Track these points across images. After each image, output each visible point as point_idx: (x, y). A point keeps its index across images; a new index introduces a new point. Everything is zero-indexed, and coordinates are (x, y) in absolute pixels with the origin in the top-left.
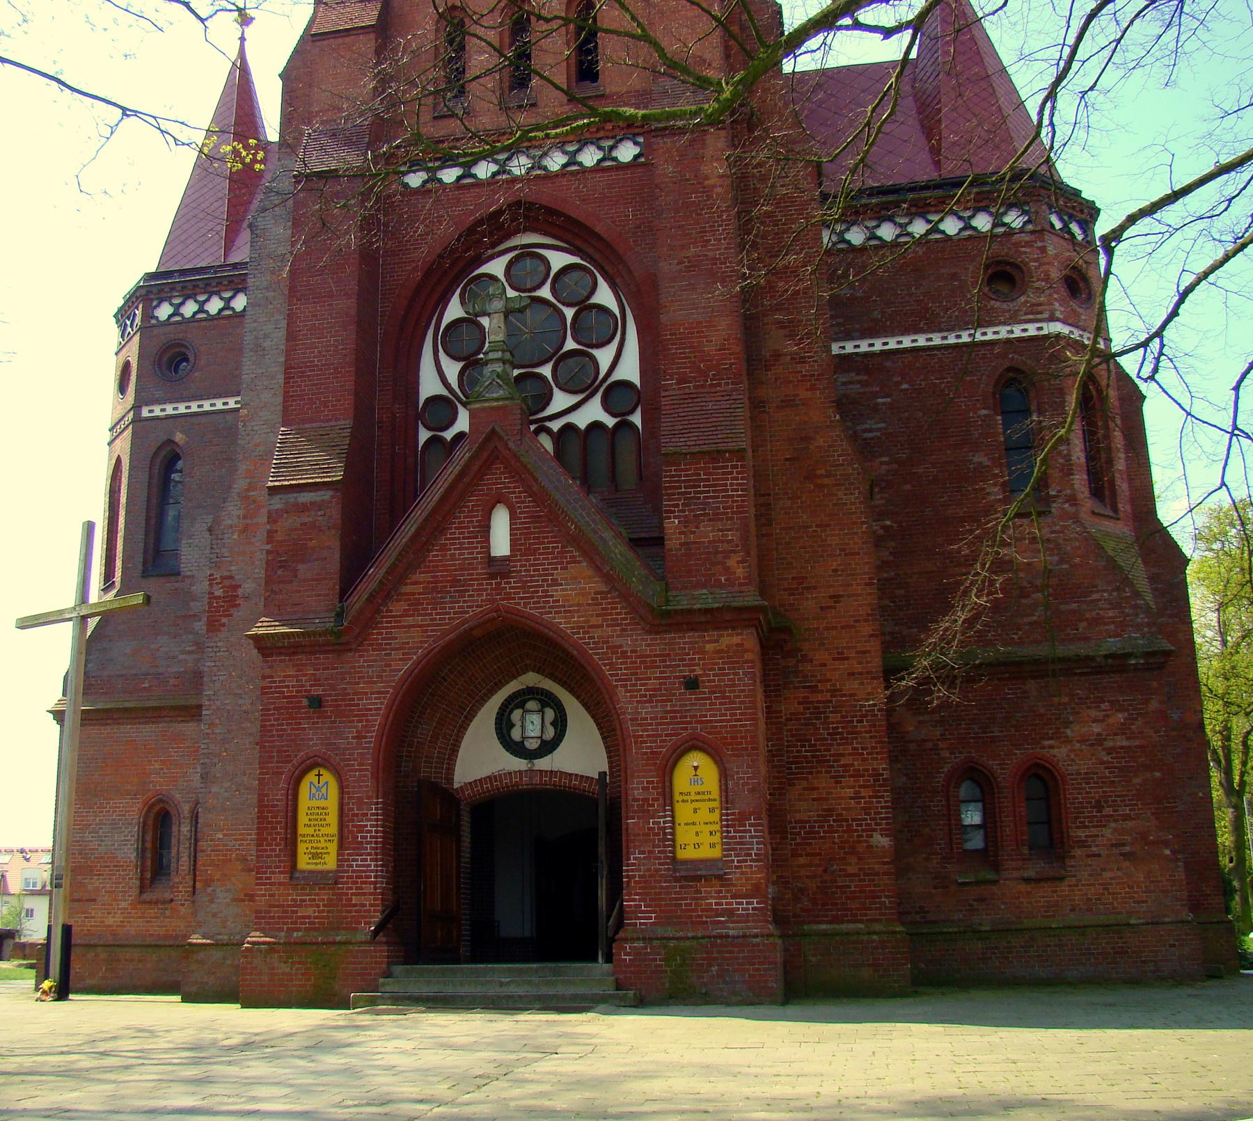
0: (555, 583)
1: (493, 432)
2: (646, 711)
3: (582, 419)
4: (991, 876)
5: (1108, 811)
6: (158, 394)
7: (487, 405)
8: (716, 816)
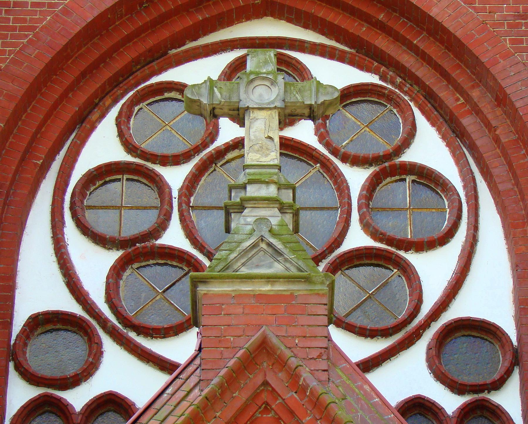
1: (264, 347)
7: (246, 288)
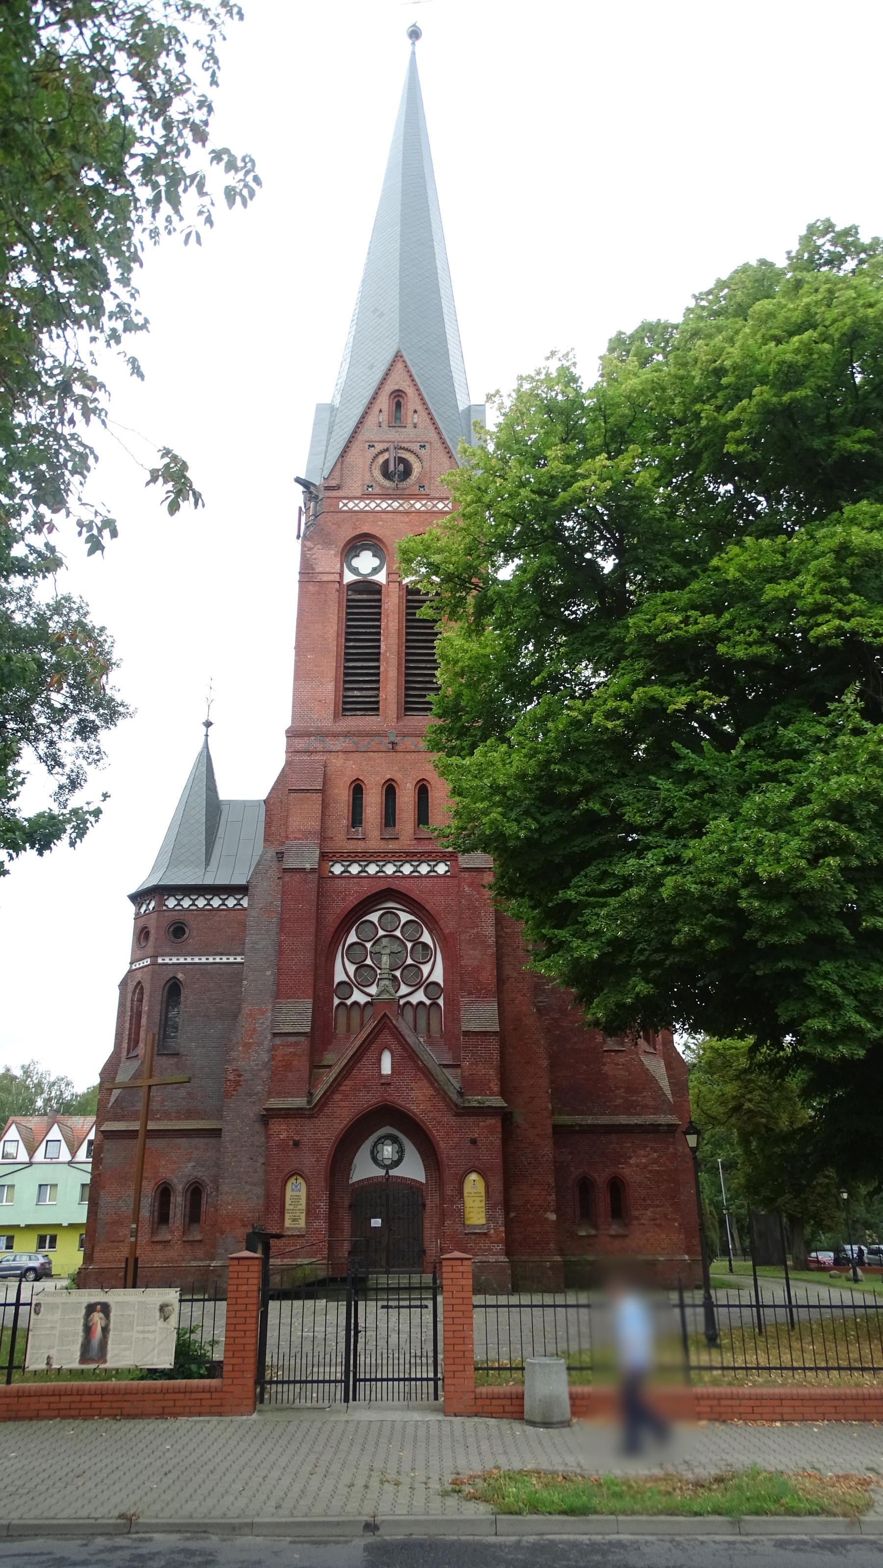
0: (412, 1089)
2: (452, 1153)
3: (415, 999)
4: (593, 1232)
5: (649, 1202)
6: (167, 950)
8: (483, 1204)
